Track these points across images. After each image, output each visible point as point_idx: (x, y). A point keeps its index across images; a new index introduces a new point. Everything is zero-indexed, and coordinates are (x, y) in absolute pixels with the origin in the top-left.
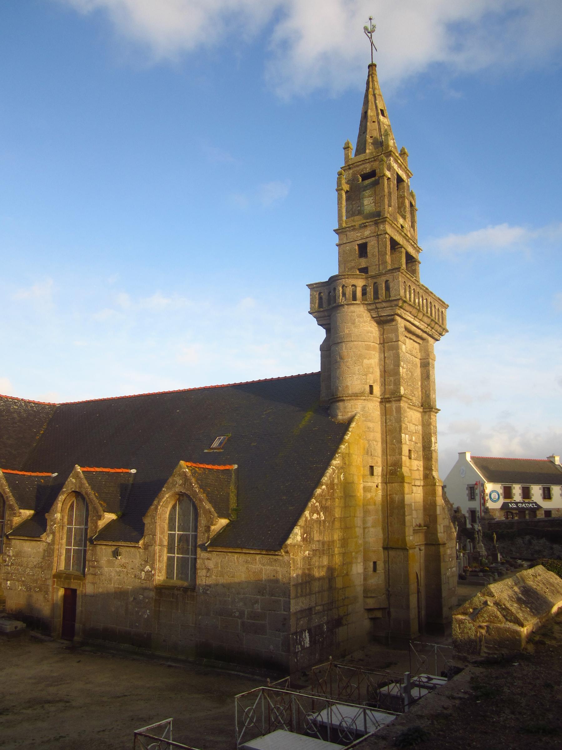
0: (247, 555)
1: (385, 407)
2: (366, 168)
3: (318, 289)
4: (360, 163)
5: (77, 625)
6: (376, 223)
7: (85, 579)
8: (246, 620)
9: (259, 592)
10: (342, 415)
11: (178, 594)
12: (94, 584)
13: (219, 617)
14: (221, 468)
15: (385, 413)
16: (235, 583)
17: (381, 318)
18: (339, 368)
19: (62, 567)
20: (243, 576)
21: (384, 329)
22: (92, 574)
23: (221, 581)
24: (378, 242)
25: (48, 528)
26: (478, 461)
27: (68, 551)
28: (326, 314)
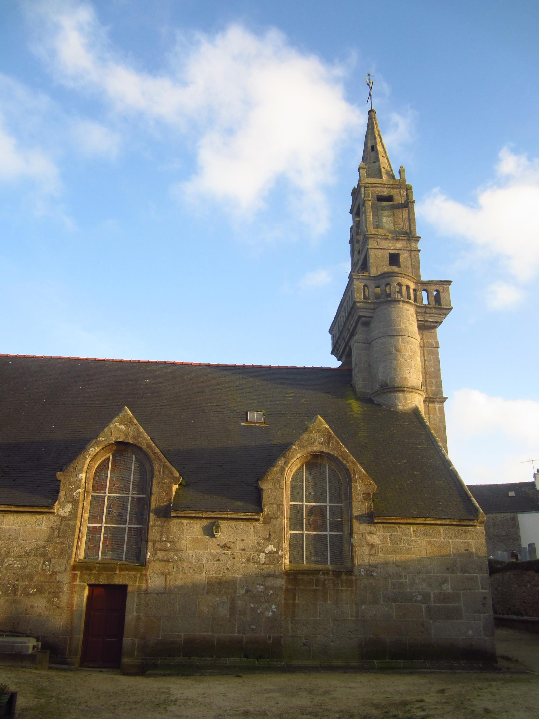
0: (428, 527)
1: (428, 406)
2: (383, 192)
3: (364, 281)
4: (378, 185)
5: (127, 641)
7: (146, 569)
8: (432, 604)
9: (448, 569)
10: (403, 406)
11: (325, 580)
12: (164, 575)
13: (394, 604)
16: (413, 560)
17: (426, 324)
18: (395, 359)
19: (81, 556)
20: (424, 551)
21: (423, 335)
22: (163, 561)
23: (392, 558)
24: (411, 255)
25: (62, 494)
27: (93, 532)
28: (372, 306)
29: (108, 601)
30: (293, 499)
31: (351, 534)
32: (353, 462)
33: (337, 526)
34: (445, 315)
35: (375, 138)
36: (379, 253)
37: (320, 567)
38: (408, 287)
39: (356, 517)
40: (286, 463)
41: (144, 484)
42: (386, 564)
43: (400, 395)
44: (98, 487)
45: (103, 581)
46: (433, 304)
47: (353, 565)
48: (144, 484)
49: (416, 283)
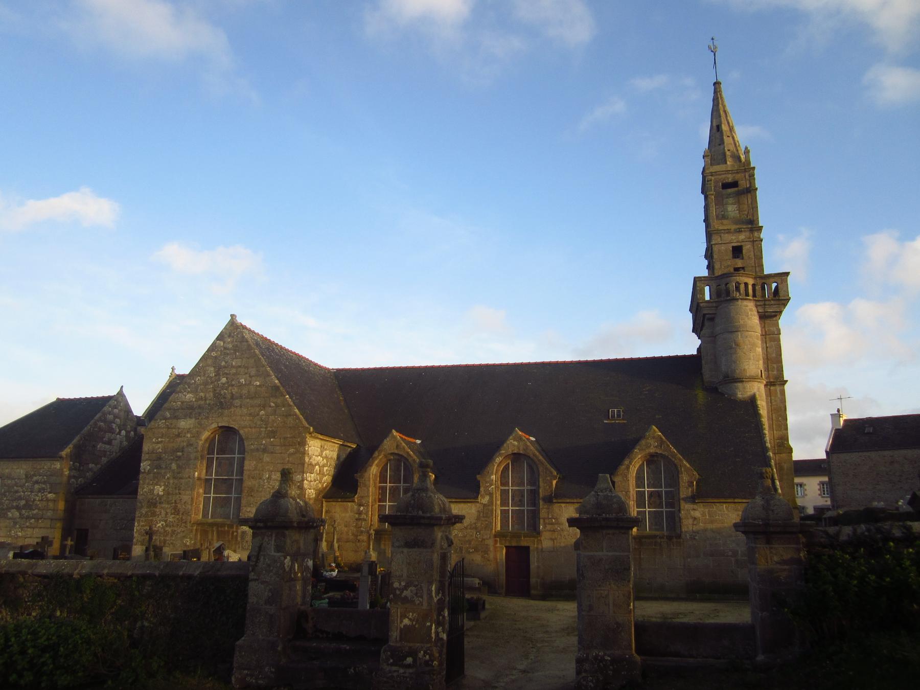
5: (533, 580)
6: (752, 230)
15: (769, 394)
19: (499, 528)
23: (710, 526)
25: (482, 489)
27: (504, 513)
29: (518, 557)
30: (638, 486)
31: (679, 511)
32: (680, 460)
33: (670, 505)
34: (785, 305)
35: (720, 116)
36: (723, 248)
37: (658, 533)
38: (746, 284)
39: (683, 499)
40: (630, 463)
41: (534, 481)
42: (705, 530)
43: (740, 385)
44: (504, 483)
45: (514, 544)
46: (771, 297)
47: (681, 532)
48: (534, 481)
49: (755, 278)
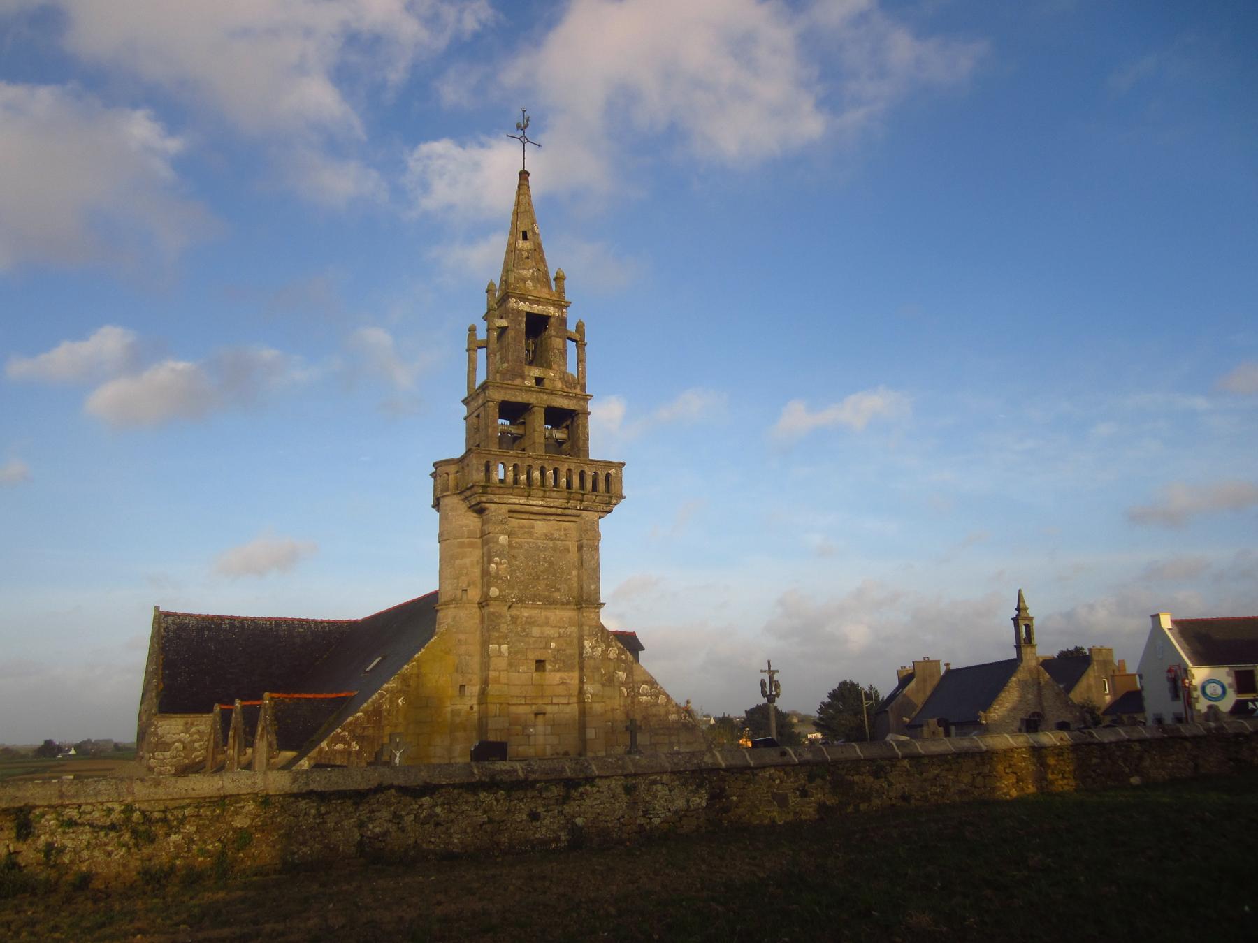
14: (334, 695)
26: (1184, 627)
